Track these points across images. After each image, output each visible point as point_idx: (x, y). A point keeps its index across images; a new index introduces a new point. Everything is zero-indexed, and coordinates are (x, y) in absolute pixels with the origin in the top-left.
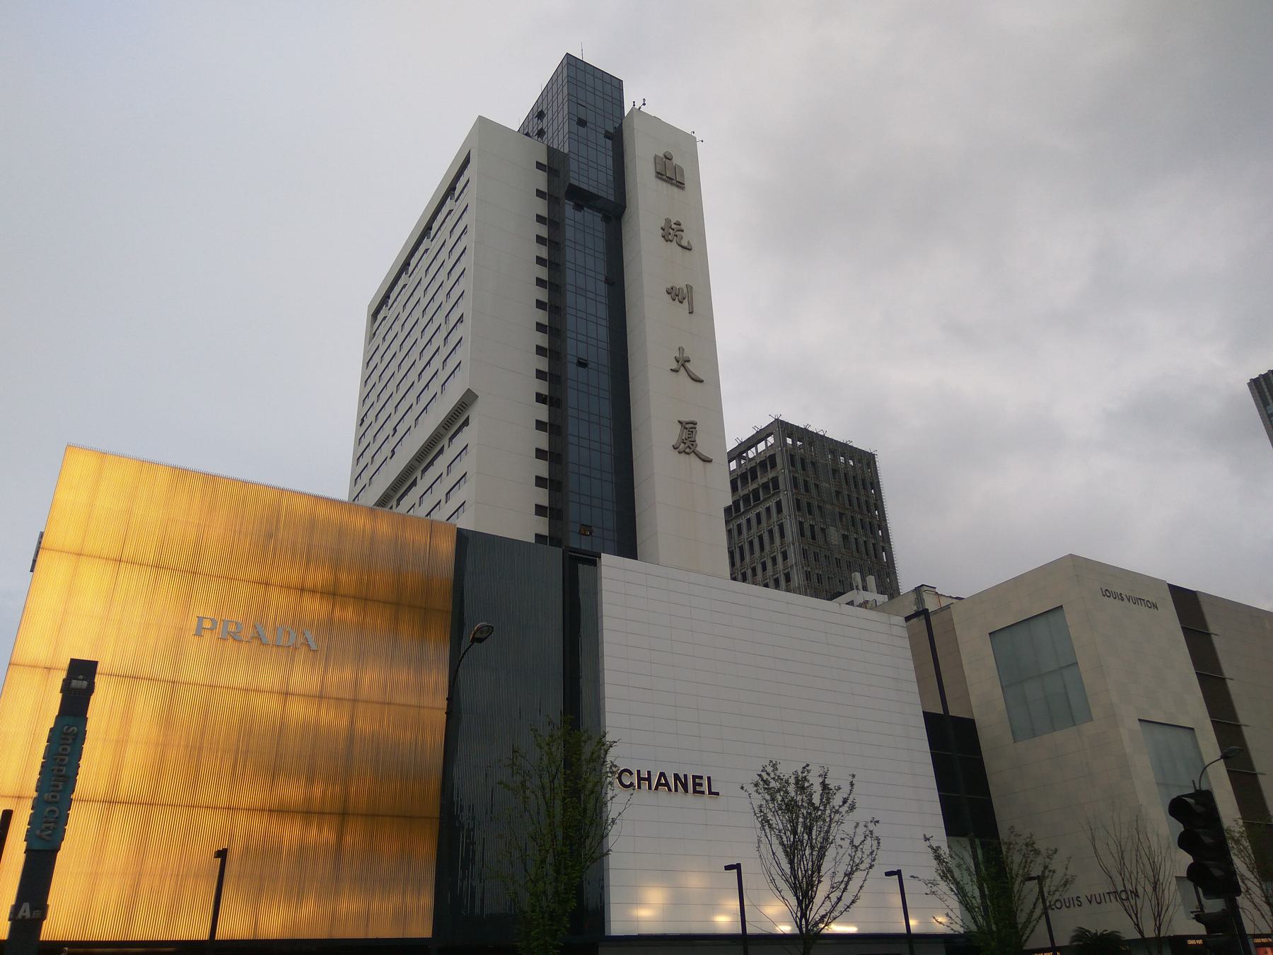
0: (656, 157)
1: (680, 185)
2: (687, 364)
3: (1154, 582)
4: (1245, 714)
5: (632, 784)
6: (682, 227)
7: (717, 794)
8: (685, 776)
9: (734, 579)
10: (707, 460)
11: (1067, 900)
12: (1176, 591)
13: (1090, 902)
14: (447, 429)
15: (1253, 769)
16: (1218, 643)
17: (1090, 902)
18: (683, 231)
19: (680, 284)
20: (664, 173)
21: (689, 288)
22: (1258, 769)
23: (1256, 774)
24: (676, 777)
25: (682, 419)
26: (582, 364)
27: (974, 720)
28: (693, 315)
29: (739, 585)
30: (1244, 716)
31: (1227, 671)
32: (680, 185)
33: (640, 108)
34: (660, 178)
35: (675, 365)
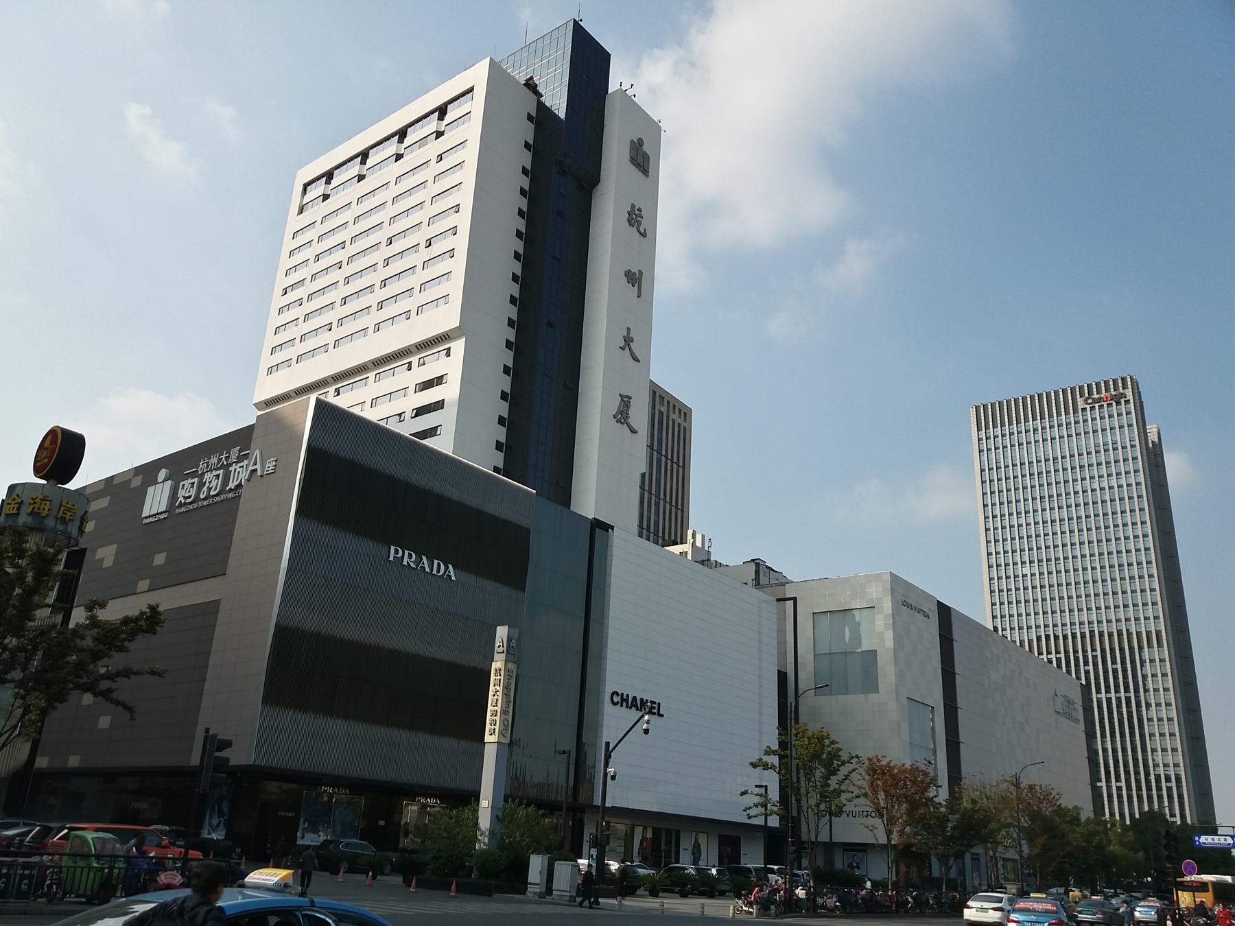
0: (632, 141)
1: (645, 172)
2: (631, 343)
3: (929, 597)
4: (961, 701)
5: (618, 702)
6: (642, 213)
7: (662, 716)
8: (628, 696)
9: (641, 535)
10: (634, 431)
11: (854, 812)
12: (940, 604)
13: (848, 815)
14: (419, 349)
15: (954, 670)
16: (958, 679)
17: (848, 815)
18: (642, 218)
19: (635, 270)
20: (642, 165)
21: (641, 273)
22: (959, 705)
23: (955, 674)
24: (642, 699)
25: (622, 393)
26: (550, 325)
27: (786, 673)
28: (640, 299)
29: (643, 541)
30: (958, 668)
31: (958, 669)
32: (645, 172)
33: (626, 90)
34: (632, 163)
35: (622, 343)
